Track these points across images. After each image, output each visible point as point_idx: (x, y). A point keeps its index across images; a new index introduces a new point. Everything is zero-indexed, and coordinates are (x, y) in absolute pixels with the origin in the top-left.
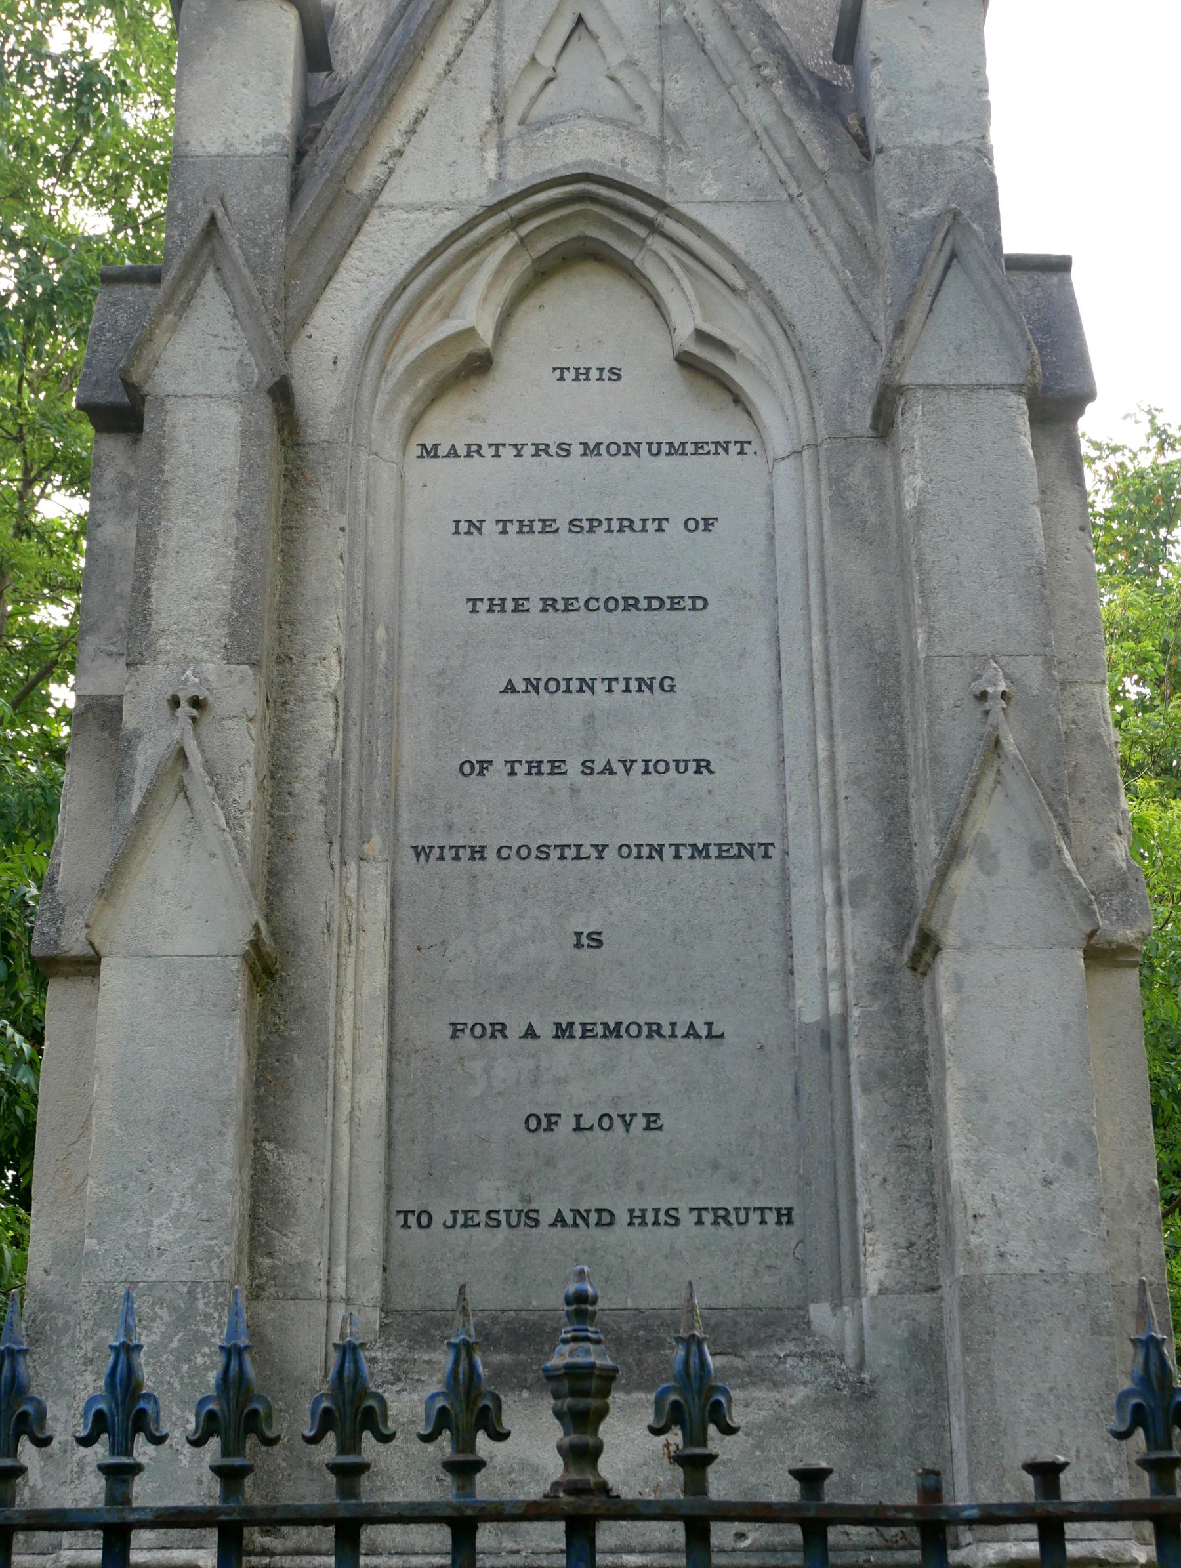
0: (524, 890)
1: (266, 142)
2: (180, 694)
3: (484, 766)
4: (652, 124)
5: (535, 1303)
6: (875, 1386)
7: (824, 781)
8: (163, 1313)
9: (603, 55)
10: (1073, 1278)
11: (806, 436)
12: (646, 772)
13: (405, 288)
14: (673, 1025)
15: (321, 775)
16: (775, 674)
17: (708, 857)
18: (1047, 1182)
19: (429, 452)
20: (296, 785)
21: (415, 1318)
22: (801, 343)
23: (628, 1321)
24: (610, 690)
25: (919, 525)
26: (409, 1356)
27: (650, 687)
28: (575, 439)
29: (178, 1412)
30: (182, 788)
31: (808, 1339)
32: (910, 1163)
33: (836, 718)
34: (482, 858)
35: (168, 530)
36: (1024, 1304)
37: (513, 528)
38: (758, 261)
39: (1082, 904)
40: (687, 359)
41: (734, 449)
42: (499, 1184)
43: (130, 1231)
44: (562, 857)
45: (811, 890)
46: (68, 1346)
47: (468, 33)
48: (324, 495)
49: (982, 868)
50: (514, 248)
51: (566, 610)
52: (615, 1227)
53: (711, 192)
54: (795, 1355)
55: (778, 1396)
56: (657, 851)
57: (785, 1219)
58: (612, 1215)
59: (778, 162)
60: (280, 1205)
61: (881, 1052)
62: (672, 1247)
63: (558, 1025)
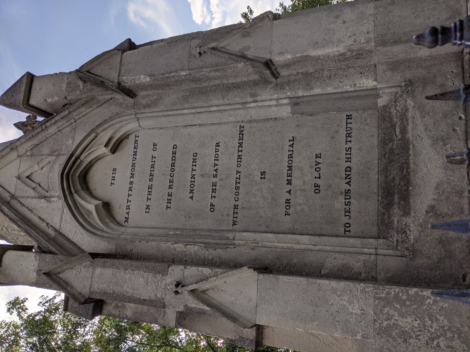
0: (247, 194)
1: (36, 260)
2: (174, 290)
3: (212, 205)
4: (53, 158)
5: (376, 191)
6: (408, 80)
7: (223, 108)
8: (386, 310)
9: (36, 171)
10: (376, 12)
11: (133, 116)
12: (218, 160)
13: (81, 223)
14: (289, 151)
15: (207, 250)
16: (195, 126)
17: (242, 143)
18: (344, 22)
19: (127, 219)
20: (210, 258)
21: (381, 229)
22: (110, 118)
23: (383, 161)
24: (195, 170)
25: (153, 75)
26: (395, 229)
27: (195, 159)
28: (129, 180)
29: (426, 306)
30: (204, 292)
31: (390, 105)
32: (335, 75)
33: (206, 105)
34: (237, 206)
35: (127, 292)
36: (384, 25)
37: (150, 197)
38: (89, 129)
39: (260, 21)
40: (113, 151)
41: (137, 139)
42: (336, 202)
43: (355, 321)
44: (239, 183)
45: (254, 112)
46: (396, 349)
47: (23, 205)
48: (129, 247)
49: (248, 50)
50: (77, 194)
51: (173, 182)
52: (351, 166)
53: (71, 142)
54: (396, 107)
55: (411, 109)
56: (239, 157)
57: (350, 117)
58: (347, 167)
59: (66, 125)
60: (343, 269)
61: (301, 86)
62: (358, 149)
63: (287, 184)
